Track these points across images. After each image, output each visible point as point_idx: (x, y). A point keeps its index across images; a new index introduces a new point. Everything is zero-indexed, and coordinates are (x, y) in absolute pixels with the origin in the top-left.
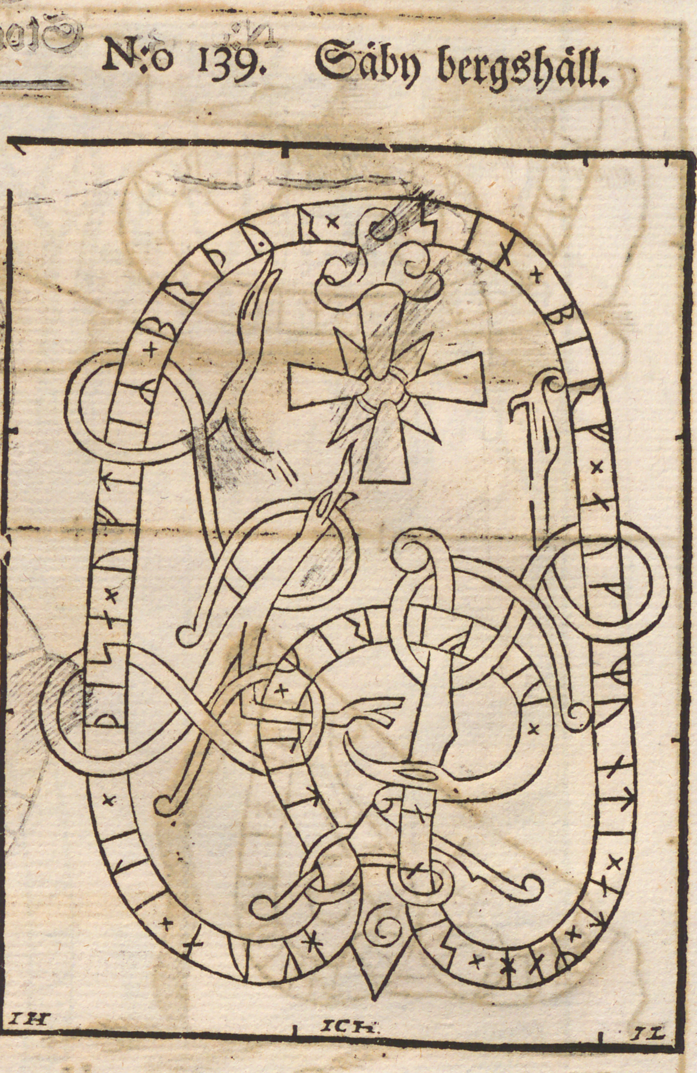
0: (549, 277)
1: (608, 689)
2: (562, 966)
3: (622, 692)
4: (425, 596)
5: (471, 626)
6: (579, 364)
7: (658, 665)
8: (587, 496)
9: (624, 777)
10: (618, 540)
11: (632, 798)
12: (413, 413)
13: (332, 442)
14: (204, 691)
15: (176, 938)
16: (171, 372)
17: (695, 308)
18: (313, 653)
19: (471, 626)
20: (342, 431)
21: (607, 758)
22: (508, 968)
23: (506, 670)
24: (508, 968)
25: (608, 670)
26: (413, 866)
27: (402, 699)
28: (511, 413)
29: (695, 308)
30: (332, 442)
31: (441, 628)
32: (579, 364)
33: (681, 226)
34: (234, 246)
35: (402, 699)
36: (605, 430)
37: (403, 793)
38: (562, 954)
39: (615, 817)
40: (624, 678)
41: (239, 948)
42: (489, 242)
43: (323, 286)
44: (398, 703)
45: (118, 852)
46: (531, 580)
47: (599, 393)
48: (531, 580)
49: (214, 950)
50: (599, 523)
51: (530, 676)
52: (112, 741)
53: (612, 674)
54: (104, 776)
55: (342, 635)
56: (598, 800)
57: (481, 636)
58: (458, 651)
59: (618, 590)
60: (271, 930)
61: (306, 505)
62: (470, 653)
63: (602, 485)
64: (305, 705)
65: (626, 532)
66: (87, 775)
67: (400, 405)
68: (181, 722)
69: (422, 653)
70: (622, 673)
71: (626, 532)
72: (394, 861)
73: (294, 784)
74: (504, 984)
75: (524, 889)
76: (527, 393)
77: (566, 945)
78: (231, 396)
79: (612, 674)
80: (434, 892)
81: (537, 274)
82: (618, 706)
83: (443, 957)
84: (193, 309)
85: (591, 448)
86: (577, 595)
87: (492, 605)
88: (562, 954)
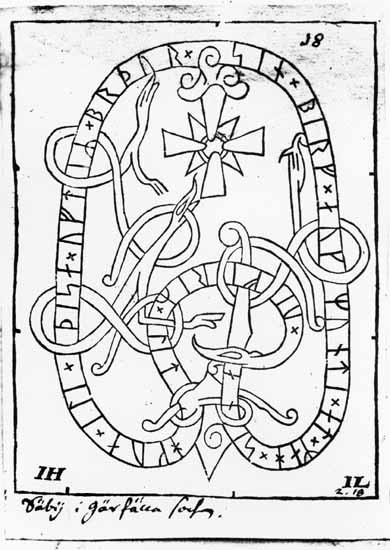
0: (302, 85)
2: (308, 459)
3: (345, 314)
4: (236, 258)
5: (259, 276)
6: (316, 132)
7: (362, 296)
8: (322, 205)
9: (343, 355)
10: (340, 227)
11: (347, 368)
12: (229, 159)
13: (187, 173)
14: (119, 308)
16: (102, 138)
18: (177, 291)
19: (259, 276)
20: (191, 169)
21: (333, 346)
22: (280, 459)
23: (276, 299)
24: (280, 459)
25: (333, 299)
26: (233, 408)
27: (224, 314)
28: (282, 155)
30: (187, 173)
31: (245, 275)
34: (134, 69)
35: (224, 314)
36: (331, 169)
37: (212, 286)
38: (308, 452)
39: (337, 378)
40: (345, 305)
42: (270, 63)
43: (182, 91)
44: (219, 317)
45: (75, 397)
46: (292, 250)
47: (90, 107)
48: (292, 250)
49: (125, 450)
50: (329, 219)
51: (293, 302)
53: (337, 302)
54: (16, 443)
55: (192, 281)
56: (327, 369)
57: (265, 280)
58: (253, 288)
61: (171, 209)
62: (260, 288)
63: (331, 199)
64: (171, 317)
65: (343, 224)
66: (55, 354)
67: (204, 141)
70: (344, 301)
71: (343, 224)
72: (218, 401)
73: (165, 359)
74: (278, 467)
75: (290, 417)
76: (292, 147)
77: (310, 446)
79: (337, 302)
80: (240, 419)
82: (142, 60)
83: (247, 452)
84: (113, 104)
88: (308, 452)
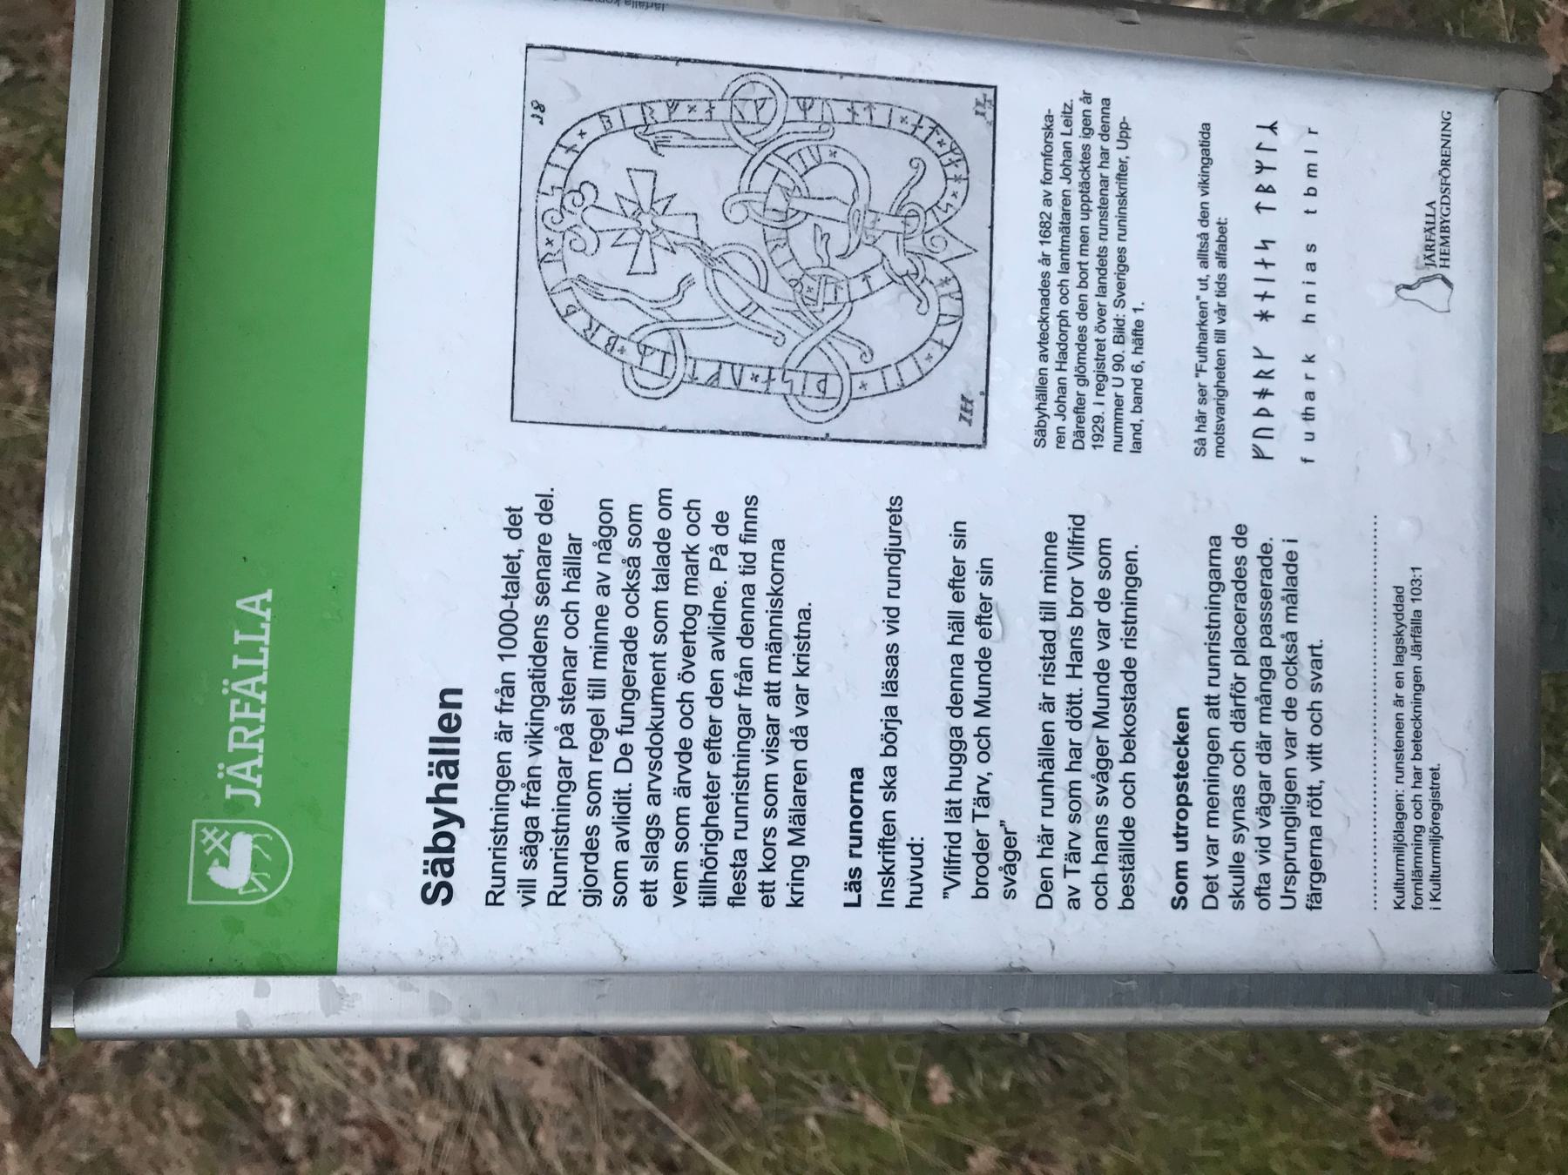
1: (814, 114)
9: (858, 108)
14: (806, 331)
15: (938, 352)
17: (1409, 1017)
18: (793, 271)
29: (1409, 1017)
31: (777, 200)
32: (633, 116)
33: (1487, 469)
34: (564, 300)
36: (673, 105)
41: (943, 320)
46: (752, 150)
50: (722, 111)
51: (805, 154)
52: (833, 383)
59: (760, 103)
60: (934, 306)
68: (824, 345)
69: (791, 213)
73: (859, 288)
78: (645, 306)
81: (582, 134)
85: (682, 111)
86: (759, 127)
87: (766, 174)
